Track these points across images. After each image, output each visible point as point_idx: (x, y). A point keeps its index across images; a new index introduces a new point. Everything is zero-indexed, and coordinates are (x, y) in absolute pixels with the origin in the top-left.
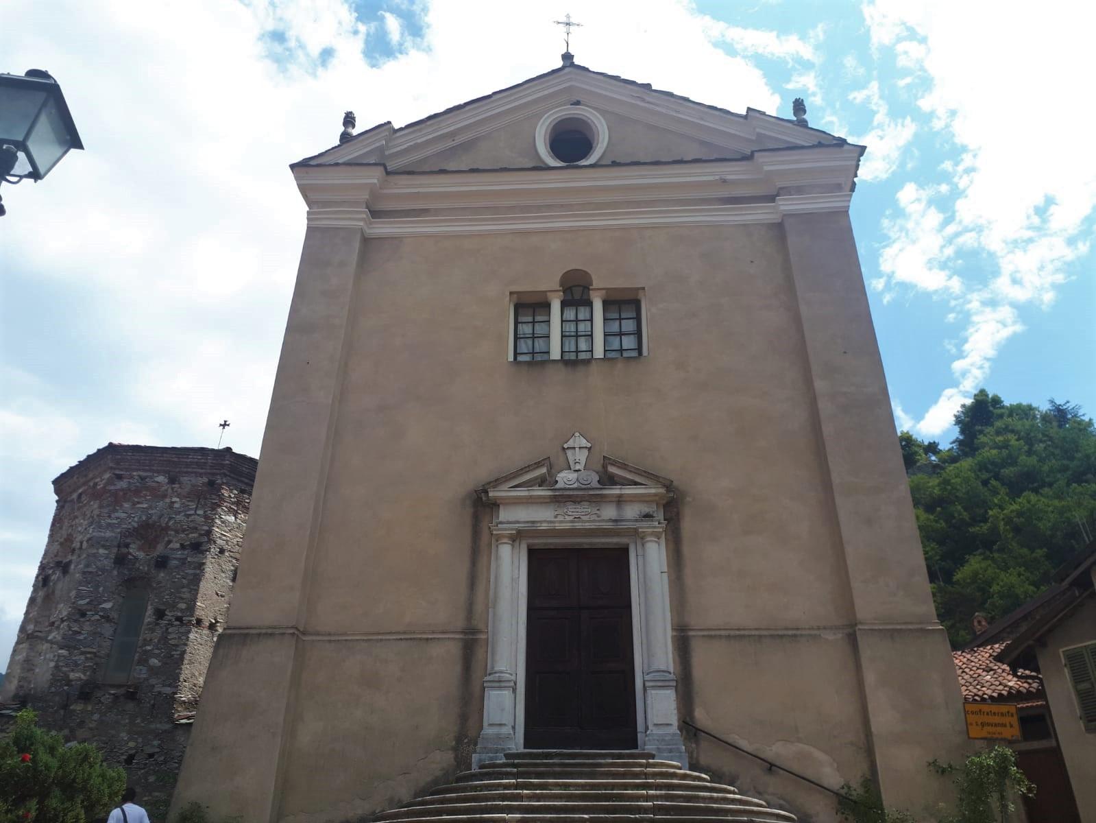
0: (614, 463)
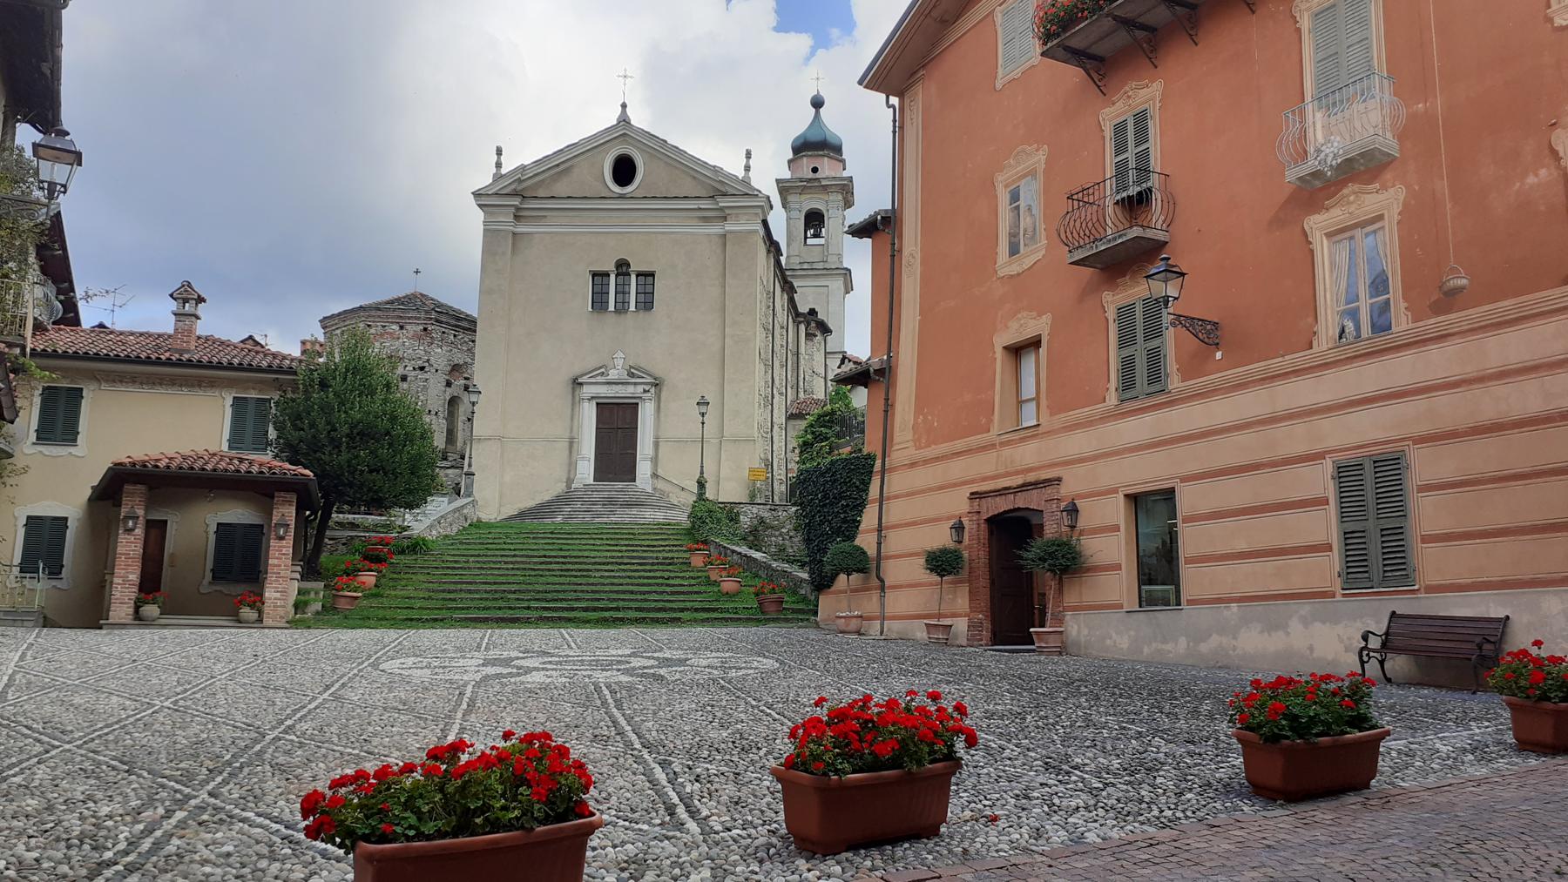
0: (633, 368)
